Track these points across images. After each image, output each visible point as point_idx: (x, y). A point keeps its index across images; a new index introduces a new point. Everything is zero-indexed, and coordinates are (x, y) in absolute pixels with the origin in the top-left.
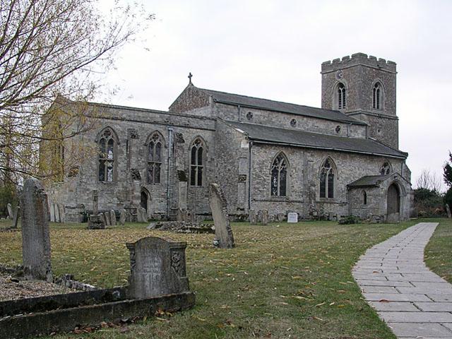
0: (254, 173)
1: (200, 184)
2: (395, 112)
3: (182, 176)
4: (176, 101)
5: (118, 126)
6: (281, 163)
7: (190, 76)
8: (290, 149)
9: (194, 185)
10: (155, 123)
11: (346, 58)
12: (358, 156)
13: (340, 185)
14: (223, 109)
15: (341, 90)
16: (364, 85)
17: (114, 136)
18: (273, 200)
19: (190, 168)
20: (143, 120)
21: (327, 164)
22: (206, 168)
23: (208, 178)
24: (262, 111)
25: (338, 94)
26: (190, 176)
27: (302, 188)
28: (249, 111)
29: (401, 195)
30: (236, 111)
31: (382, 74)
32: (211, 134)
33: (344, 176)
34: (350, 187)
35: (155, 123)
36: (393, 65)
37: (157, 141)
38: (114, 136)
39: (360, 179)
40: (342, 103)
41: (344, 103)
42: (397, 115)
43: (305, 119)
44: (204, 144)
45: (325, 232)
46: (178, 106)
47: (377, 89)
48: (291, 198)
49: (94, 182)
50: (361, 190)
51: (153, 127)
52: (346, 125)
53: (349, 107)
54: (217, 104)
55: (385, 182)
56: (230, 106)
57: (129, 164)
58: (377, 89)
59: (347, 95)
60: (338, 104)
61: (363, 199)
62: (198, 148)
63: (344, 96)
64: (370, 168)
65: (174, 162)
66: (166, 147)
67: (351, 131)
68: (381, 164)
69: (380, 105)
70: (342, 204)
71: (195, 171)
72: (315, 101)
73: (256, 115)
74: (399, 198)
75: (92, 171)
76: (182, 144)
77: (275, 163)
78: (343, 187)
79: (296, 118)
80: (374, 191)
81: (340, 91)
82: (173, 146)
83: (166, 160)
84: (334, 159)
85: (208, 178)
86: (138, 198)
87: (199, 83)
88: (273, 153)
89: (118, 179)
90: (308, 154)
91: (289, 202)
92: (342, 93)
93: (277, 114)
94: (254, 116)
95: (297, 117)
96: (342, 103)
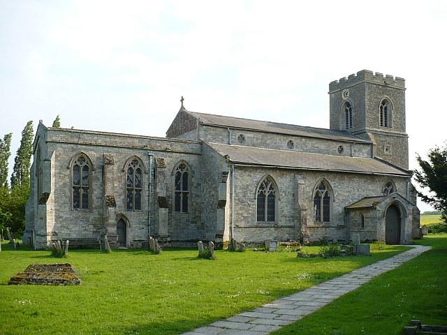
0: (237, 198)
1: (185, 210)
2: (404, 130)
3: (162, 202)
4: (172, 126)
5: (93, 154)
6: (269, 186)
7: (182, 100)
8: (278, 171)
9: (179, 210)
10: (133, 148)
11: (351, 77)
12: (338, 176)
13: (337, 208)
14: (212, 132)
15: (348, 109)
16: (366, 104)
17: (89, 163)
18: (260, 225)
19: (174, 194)
20: (119, 145)
21: (323, 186)
22: (192, 194)
23: (194, 204)
24: (255, 133)
25: (345, 113)
26: (174, 202)
27: (293, 212)
28: (241, 133)
29: (402, 216)
30: (225, 134)
31: (389, 91)
32: (197, 158)
33: (341, 198)
34: (347, 211)
35: (133, 148)
36: (401, 81)
37: (137, 167)
38: (89, 163)
39: (360, 201)
40: (349, 122)
41: (351, 123)
42: (408, 131)
43: (304, 140)
44: (189, 169)
45: (405, 256)
46: (174, 131)
47: (384, 107)
48: (280, 224)
49: (67, 209)
50: (358, 212)
51: (132, 153)
52: (348, 145)
53: (355, 126)
54: (205, 127)
55: (383, 203)
56: (218, 129)
57: (104, 191)
58: (384, 107)
59: (353, 114)
60: (345, 125)
61: (360, 221)
62: (182, 173)
63: (351, 115)
64: (371, 188)
65: (155, 188)
66: (145, 173)
67: (355, 151)
68: (383, 183)
69: (388, 123)
70: (339, 227)
71: (180, 197)
72: (324, 122)
73: (248, 137)
74: (399, 220)
75: (64, 198)
76: (163, 169)
77: (262, 187)
78: (341, 209)
79: (293, 139)
80: (371, 214)
81: (346, 110)
82: (154, 172)
83: (146, 186)
84: (330, 181)
85: (194, 204)
86: (114, 225)
87: (191, 108)
88: (259, 176)
89: (94, 206)
90: (300, 176)
91: (277, 227)
92: (349, 113)
93: (272, 136)
94: (246, 138)
95: (294, 138)
96: (349, 122)
